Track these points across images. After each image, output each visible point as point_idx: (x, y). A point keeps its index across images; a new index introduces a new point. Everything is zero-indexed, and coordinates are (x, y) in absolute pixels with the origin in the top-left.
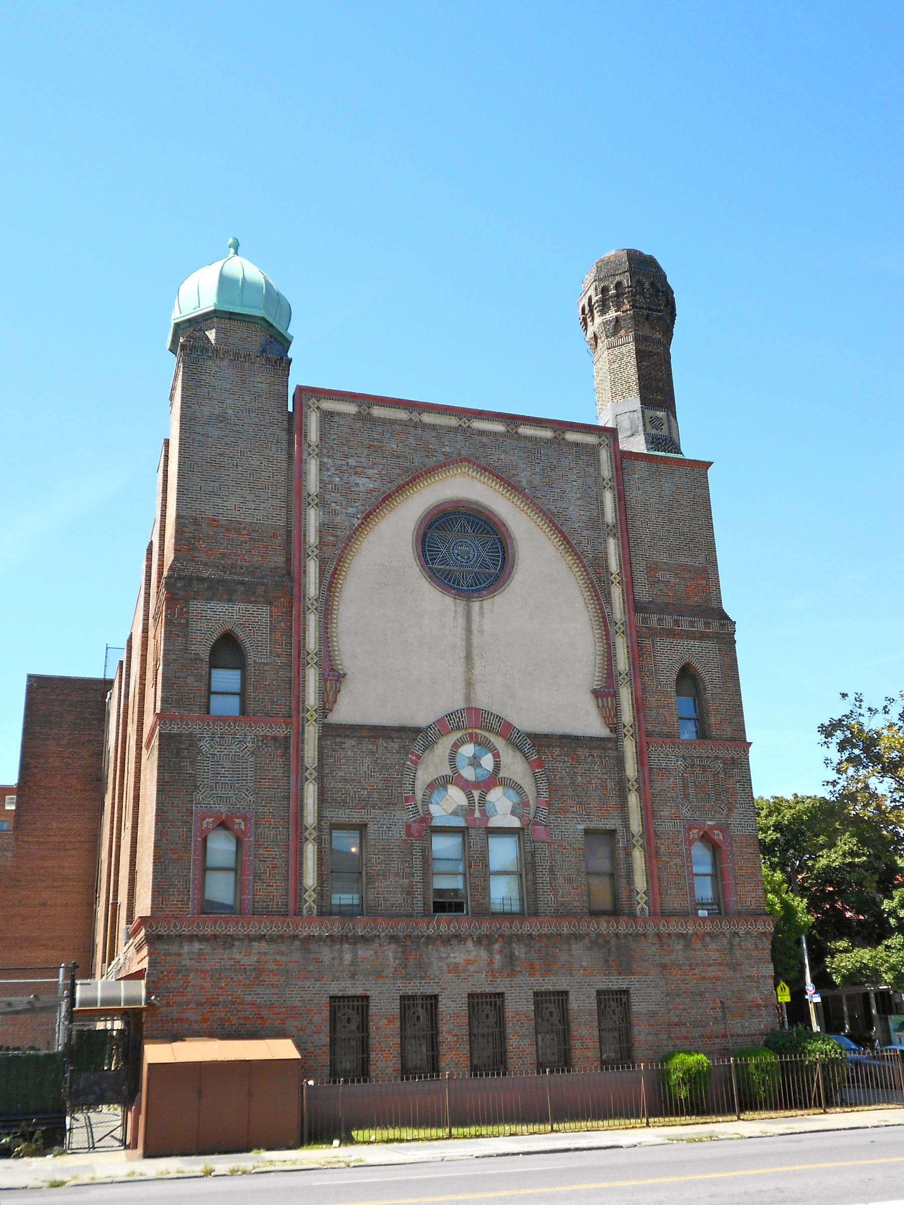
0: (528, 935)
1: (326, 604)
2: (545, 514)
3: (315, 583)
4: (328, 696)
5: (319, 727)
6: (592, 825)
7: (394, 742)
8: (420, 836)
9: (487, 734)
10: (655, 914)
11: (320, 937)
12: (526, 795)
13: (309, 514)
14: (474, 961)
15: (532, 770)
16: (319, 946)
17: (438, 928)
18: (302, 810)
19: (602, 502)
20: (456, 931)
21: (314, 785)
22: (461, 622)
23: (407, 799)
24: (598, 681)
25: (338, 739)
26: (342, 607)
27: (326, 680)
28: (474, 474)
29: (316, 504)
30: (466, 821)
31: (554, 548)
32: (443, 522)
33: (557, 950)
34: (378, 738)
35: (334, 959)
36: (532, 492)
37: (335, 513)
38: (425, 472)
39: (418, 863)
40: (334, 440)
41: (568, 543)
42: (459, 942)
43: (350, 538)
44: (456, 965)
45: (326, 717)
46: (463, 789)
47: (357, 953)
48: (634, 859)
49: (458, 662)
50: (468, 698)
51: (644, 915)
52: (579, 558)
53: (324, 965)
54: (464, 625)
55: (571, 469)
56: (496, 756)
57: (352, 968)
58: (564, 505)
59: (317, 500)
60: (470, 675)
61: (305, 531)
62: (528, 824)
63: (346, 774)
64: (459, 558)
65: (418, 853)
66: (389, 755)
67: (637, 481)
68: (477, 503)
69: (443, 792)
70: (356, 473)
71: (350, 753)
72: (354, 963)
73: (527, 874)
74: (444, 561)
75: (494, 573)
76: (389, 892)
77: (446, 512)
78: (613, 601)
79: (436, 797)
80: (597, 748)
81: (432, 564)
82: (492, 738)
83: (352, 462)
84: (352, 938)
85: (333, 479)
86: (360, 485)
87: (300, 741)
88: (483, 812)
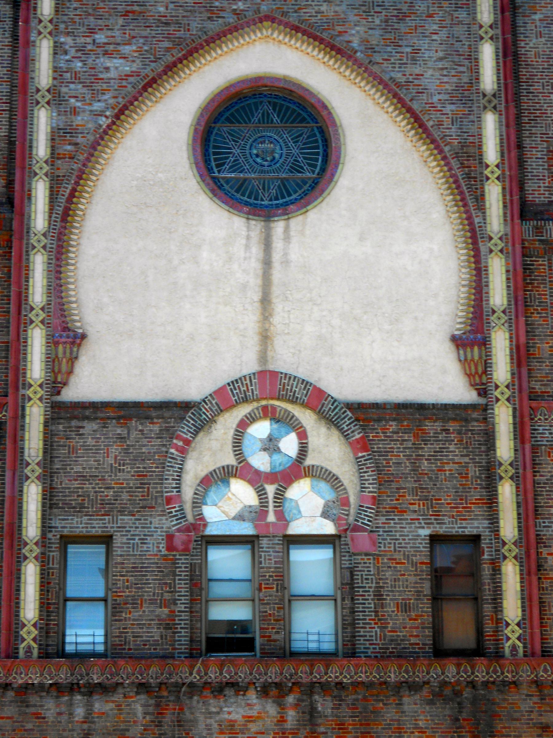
0: (337, 684)
1: (59, 239)
2: (386, 86)
3: (35, 212)
4: (60, 364)
5: (46, 407)
6: (442, 530)
7: (153, 423)
8: (186, 549)
9: (290, 407)
10: (533, 654)
11: (41, 686)
12: (345, 489)
13: (38, 118)
14: (258, 717)
15: (355, 454)
16: (41, 697)
17: (206, 674)
18: (20, 519)
19: (477, 60)
20: (231, 677)
21: (37, 485)
22: (256, 251)
23: (169, 500)
24: (460, 323)
25: (74, 423)
26: (84, 242)
27: (56, 344)
28: (281, 37)
29: (48, 103)
30: (256, 526)
31: (402, 134)
32: (237, 111)
33: (381, 705)
34: (131, 419)
35: (60, 714)
36: (368, 56)
37: (75, 111)
38: (206, 41)
39: (183, 587)
40: (76, 9)
41: (422, 125)
42: (237, 694)
43: (94, 146)
44: (232, 724)
45: (59, 393)
46: (251, 482)
47: (92, 706)
48: (504, 576)
49: (250, 308)
50: (263, 357)
51: (516, 655)
52: (437, 147)
53: (47, 722)
54: (261, 255)
55: (430, 16)
56: (302, 435)
57: (85, 726)
58: (417, 71)
59: (49, 97)
60: (267, 326)
61: (31, 140)
62: (347, 530)
63: (84, 468)
64: (259, 160)
65: (183, 571)
66: (145, 442)
67: (538, 23)
68: (285, 79)
69: (223, 488)
70: (106, 53)
71: (90, 441)
72: (88, 719)
73: (343, 599)
74: (236, 167)
75: (309, 178)
76: (141, 626)
77: (241, 96)
78: (487, 205)
79: (212, 495)
80: (454, 420)
81: (219, 172)
82: (297, 412)
83: (101, 38)
84: (84, 686)
85: (72, 65)
86: (112, 69)
87: (19, 428)
88: (280, 515)
